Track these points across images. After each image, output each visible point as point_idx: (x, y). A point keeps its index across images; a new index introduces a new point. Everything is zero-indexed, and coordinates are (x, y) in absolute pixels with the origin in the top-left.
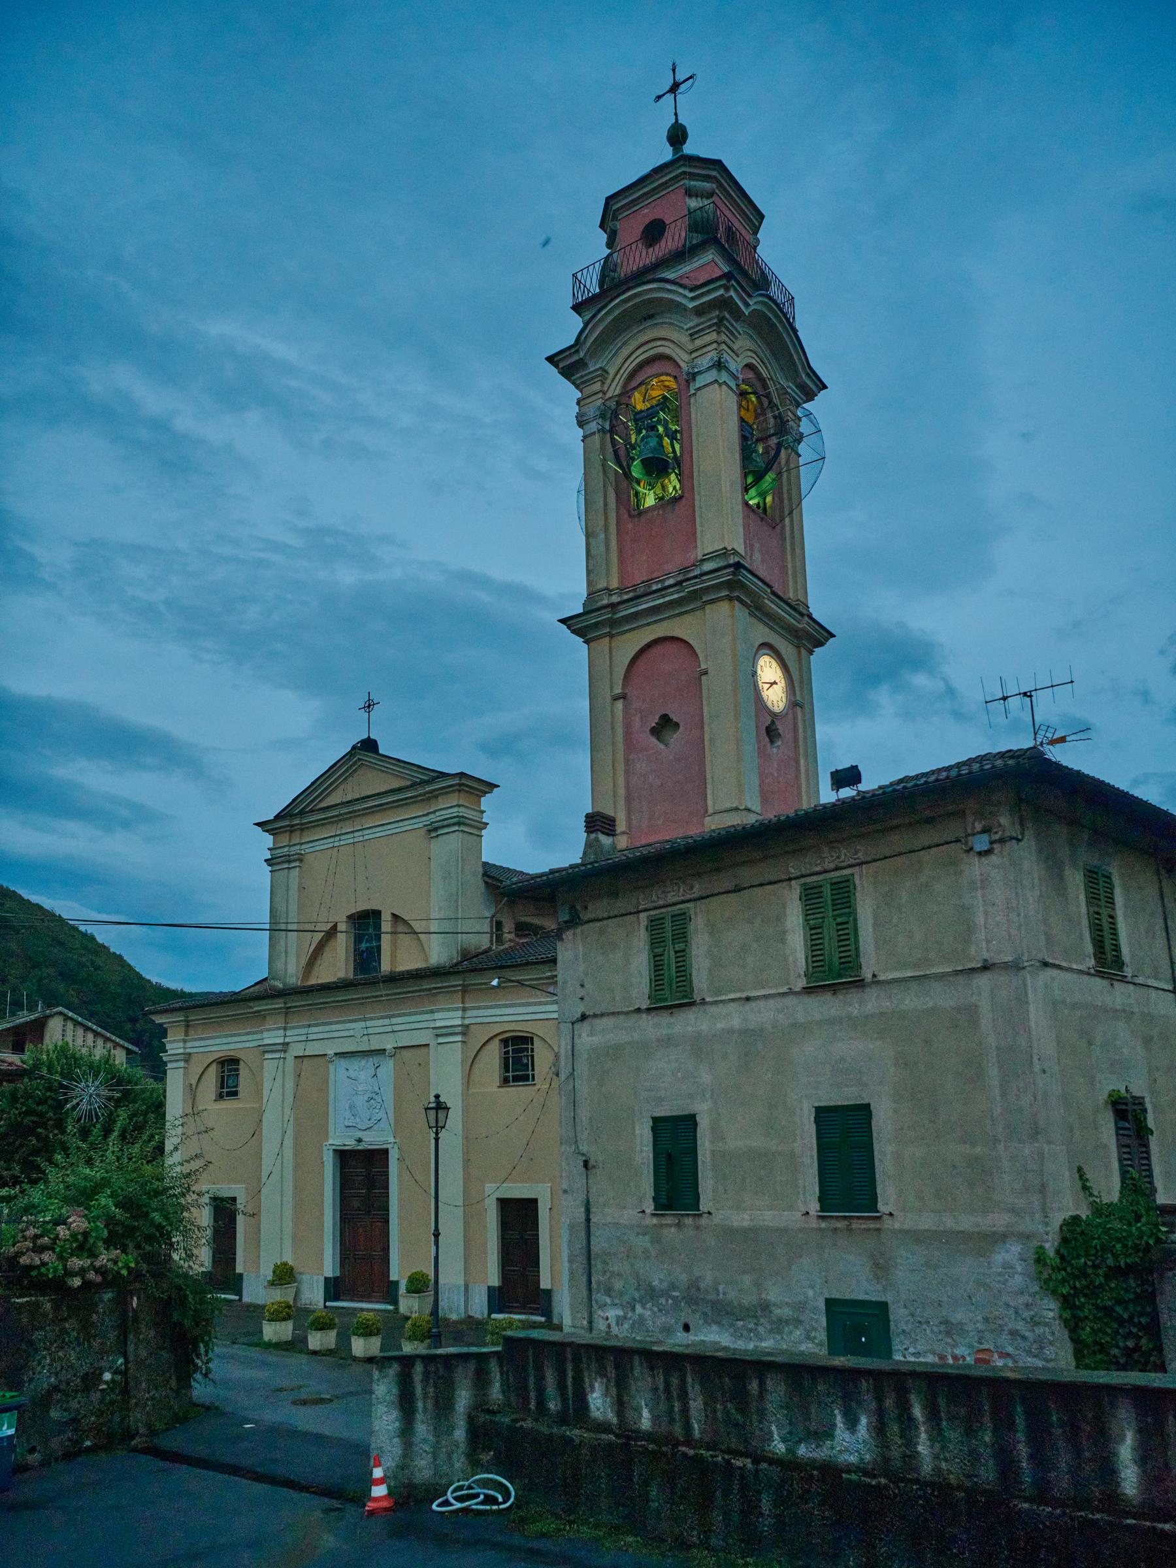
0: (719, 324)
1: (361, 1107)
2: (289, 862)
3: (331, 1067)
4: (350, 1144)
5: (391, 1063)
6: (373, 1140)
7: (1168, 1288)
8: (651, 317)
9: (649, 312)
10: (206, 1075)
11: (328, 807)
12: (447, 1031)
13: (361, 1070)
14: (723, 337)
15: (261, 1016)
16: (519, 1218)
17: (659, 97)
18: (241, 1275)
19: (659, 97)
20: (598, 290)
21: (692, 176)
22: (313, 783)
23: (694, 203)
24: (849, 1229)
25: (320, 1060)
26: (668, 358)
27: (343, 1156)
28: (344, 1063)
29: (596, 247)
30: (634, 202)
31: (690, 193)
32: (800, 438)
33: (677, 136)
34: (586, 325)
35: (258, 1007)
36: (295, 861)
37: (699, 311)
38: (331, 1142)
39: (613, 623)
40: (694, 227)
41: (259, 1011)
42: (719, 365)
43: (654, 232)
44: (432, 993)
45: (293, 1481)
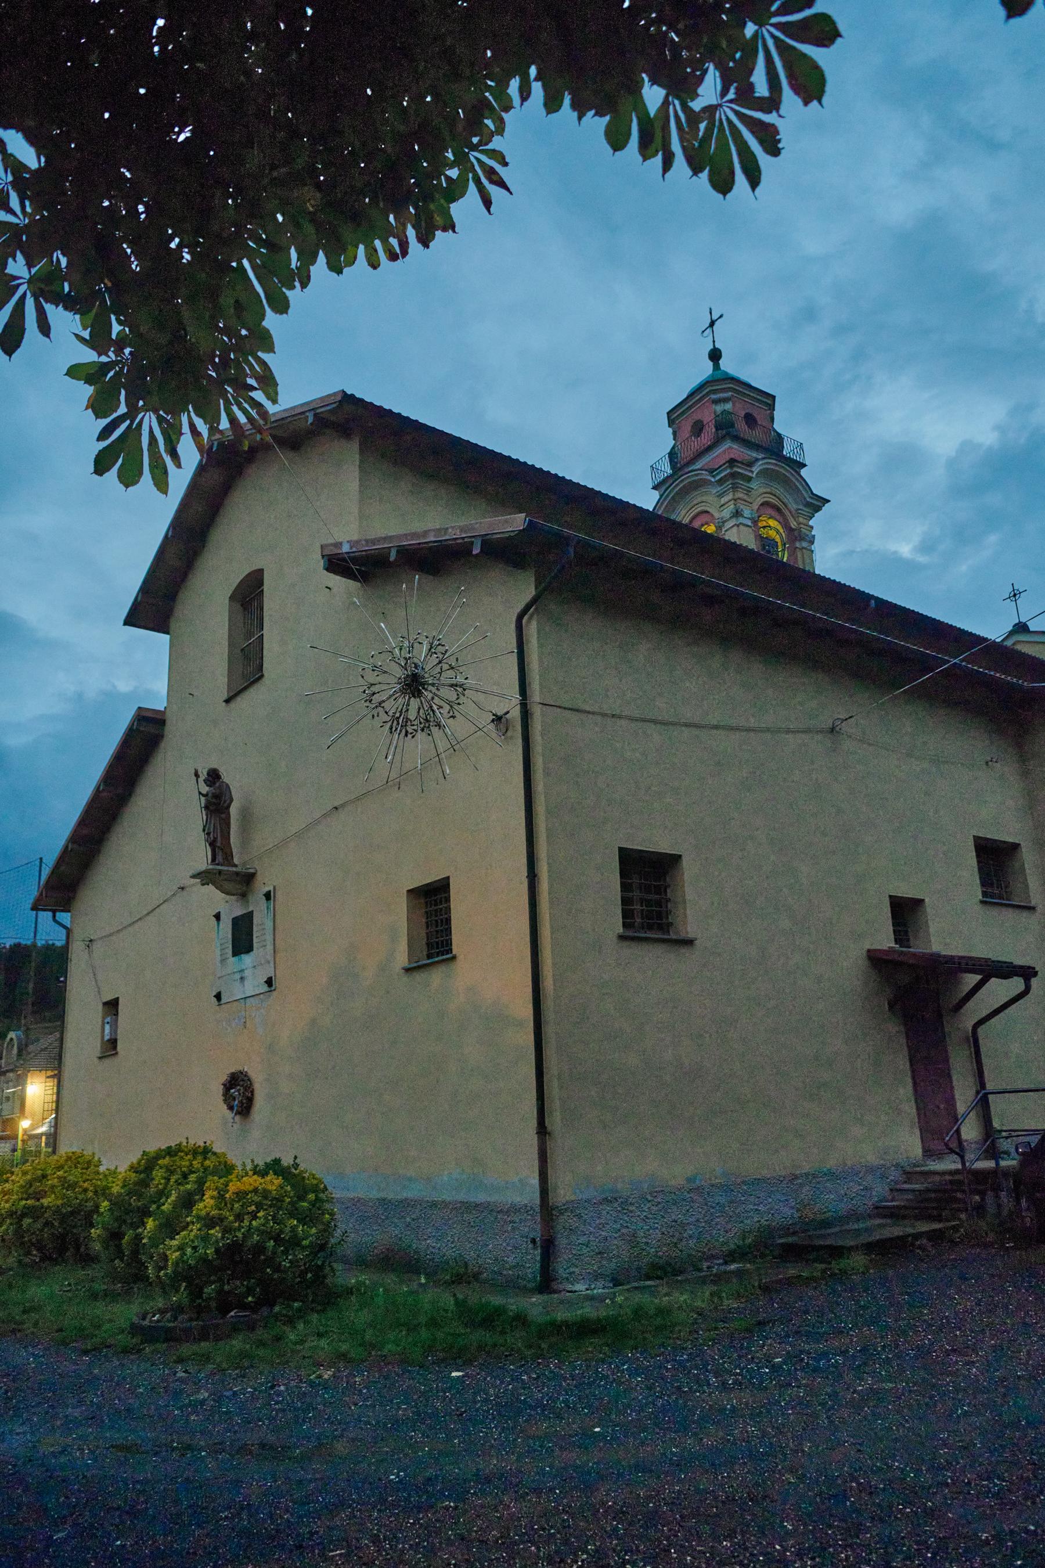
0: (735, 488)
7: (192, 1142)
9: (697, 485)
14: (740, 495)
17: (721, 316)
20: (670, 471)
21: (715, 392)
23: (719, 408)
26: (707, 512)
29: (666, 440)
30: (683, 413)
31: (716, 402)
32: (53, 944)
33: (715, 355)
34: (661, 496)
37: (720, 482)
40: (718, 427)
42: (737, 514)
43: (698, 428)
45: (543, 1077)
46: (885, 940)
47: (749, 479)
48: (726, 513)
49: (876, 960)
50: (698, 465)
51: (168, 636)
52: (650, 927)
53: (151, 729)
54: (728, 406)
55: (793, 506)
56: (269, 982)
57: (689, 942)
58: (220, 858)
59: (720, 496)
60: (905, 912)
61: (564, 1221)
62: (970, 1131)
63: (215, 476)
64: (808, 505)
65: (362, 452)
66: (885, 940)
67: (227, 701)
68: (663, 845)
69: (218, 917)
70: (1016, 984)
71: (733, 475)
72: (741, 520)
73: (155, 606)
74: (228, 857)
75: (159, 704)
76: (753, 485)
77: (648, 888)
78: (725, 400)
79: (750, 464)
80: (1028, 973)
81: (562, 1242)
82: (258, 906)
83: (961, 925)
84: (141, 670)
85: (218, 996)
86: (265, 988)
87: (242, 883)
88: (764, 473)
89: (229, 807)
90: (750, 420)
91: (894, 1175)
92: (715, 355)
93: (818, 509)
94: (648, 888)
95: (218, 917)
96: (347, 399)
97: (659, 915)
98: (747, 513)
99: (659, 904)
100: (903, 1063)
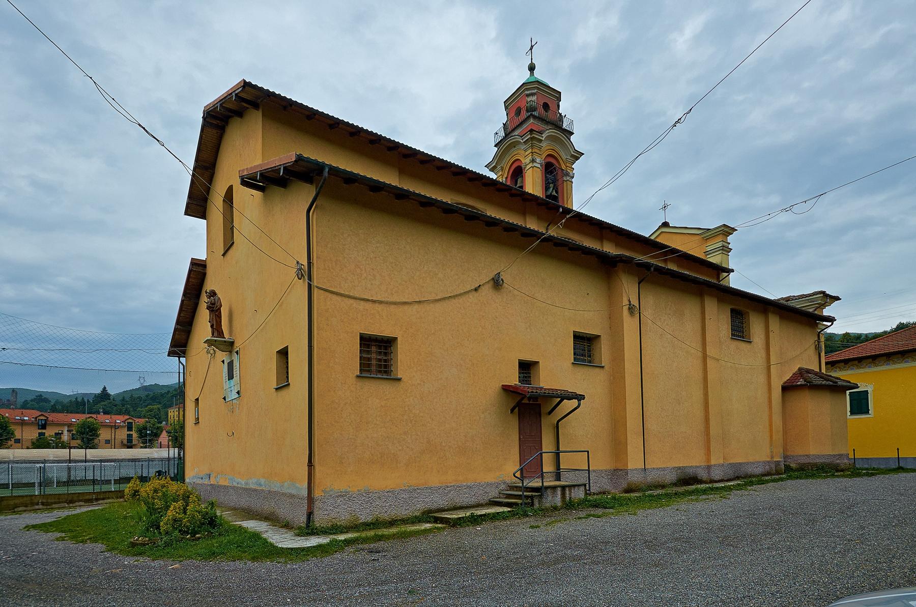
9: (514, 145)
31: (528, 95)
33: (532, 68)
42: (533, 161)
43: (518, 111)
46: (513, 379)
47: (541, 141)
48: (528, 161)
49: (506, 389)
50: (516, 133)
51: (204, 222)
52: (380, 372)
53: (200, 269)
54: (534, 98)
55: (564, 157)
56: (238, 393)
57: (400, 380)
58: (216, 334)
59: (525, 151)
60: (526, 367)
61: (318, 504)
62: (548, 467)
63: (213, 132)
64: (572, 156)
65: (263, 115)
66: (513, 379)
67: (224, 255)
68: (387, 333)
69: (223, 362)
70: (574, 403)
71: (532, 139)
72: (535, 164)
73: (197, 205)
74: (221, 334)
75: (203, 256)
76: (544, 144)
77: (377, 355)
78: (532, 94)
79: (541, 133)
80: (580, 398)
81: (316, 512)
82: (235, 358)
83: (557, 372)
84: (194, 238)
85: (224, 398)
86: (237, 396)
87: (229, 346)
88: (548, 137)
89: (219, 309)
90: (546, 106)
91: (503, 487)
92: (532, 68)
93: (577, 158)
94: (377, 355)
95: (223, 362)
96: (246, 85)
97: (386, 366)
98: (538, 160)
99: (385, 361)
100: (515, 437)
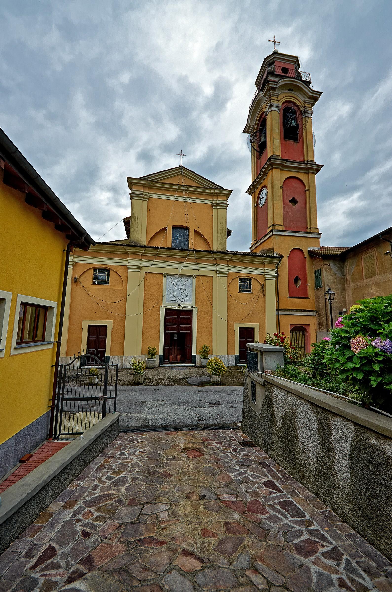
1: (179, 293)
2: (143, 198)
3: (164, 279)
4: (174, 306)
5: (194, 280)
6: (185, 306)
8: (292, 90)
10: (86, 273)
11: (163, 183)
12: (223, 273)
13: (180, 281)
15: (128, 254)
16: (246, 334)
18: (108, 357)
19: (270, 41)
22: (169, 170)
24: (53, 366)
25: (161, 275)
27: (168, 312)
28: (169, 278)
35: (128, 249)
36: (146, 198)
38: (163, 305)
39: (283, 166)
41: (127, 252)
44: (216, 260)
